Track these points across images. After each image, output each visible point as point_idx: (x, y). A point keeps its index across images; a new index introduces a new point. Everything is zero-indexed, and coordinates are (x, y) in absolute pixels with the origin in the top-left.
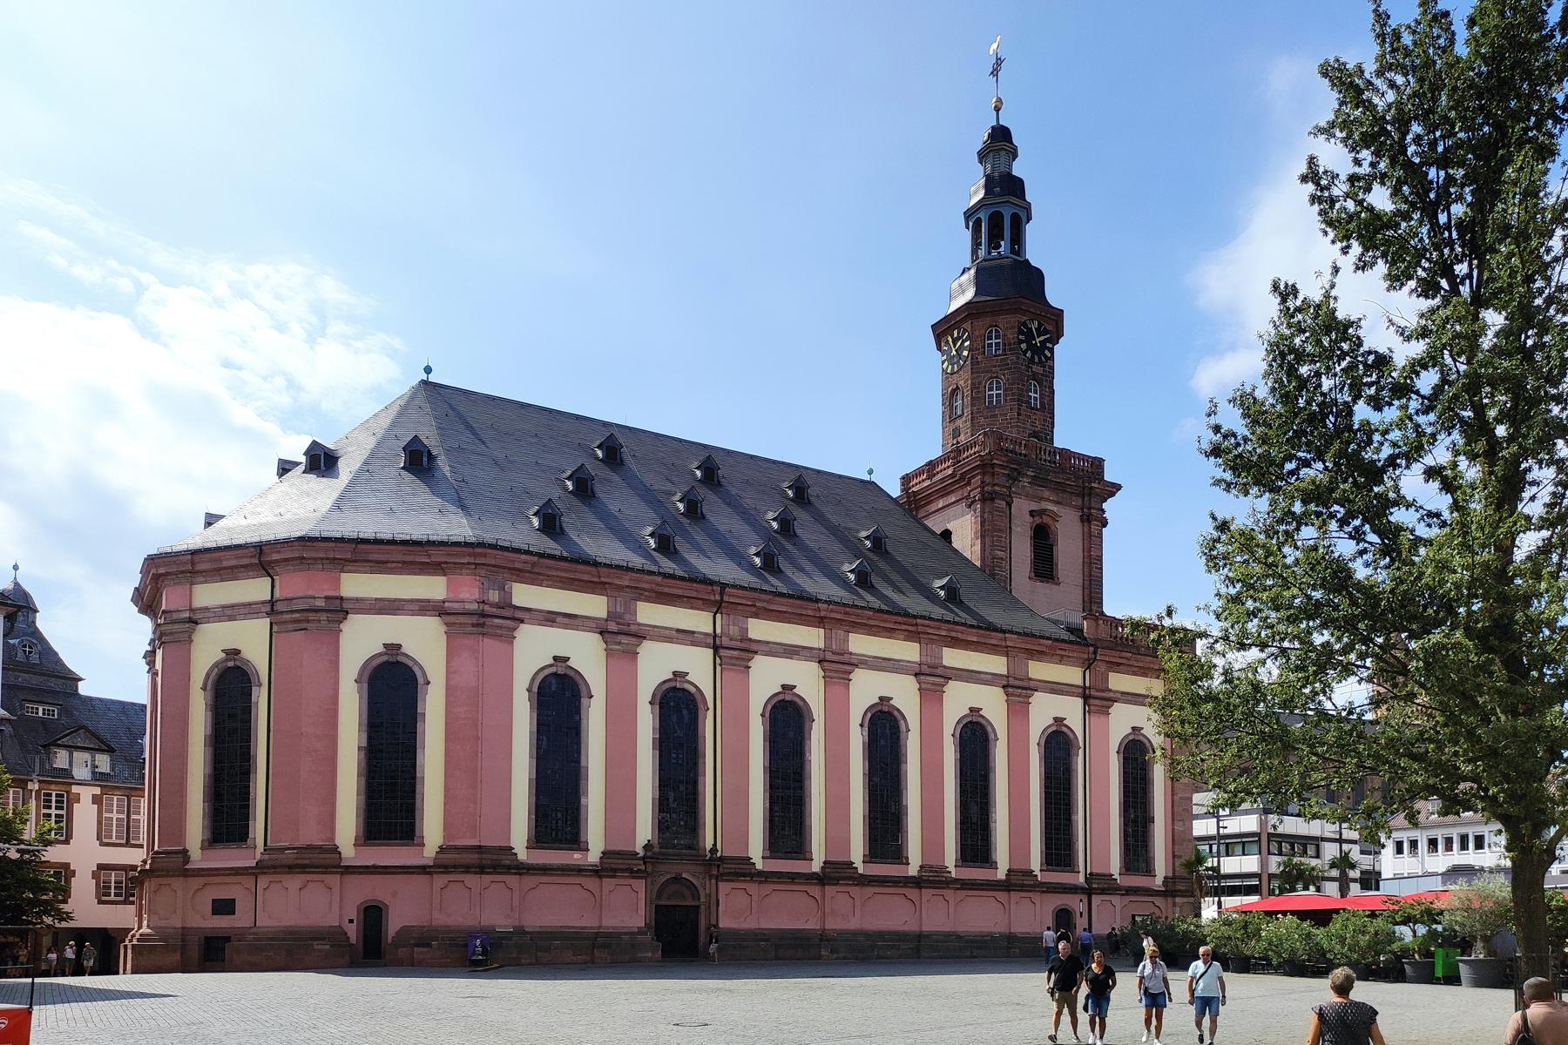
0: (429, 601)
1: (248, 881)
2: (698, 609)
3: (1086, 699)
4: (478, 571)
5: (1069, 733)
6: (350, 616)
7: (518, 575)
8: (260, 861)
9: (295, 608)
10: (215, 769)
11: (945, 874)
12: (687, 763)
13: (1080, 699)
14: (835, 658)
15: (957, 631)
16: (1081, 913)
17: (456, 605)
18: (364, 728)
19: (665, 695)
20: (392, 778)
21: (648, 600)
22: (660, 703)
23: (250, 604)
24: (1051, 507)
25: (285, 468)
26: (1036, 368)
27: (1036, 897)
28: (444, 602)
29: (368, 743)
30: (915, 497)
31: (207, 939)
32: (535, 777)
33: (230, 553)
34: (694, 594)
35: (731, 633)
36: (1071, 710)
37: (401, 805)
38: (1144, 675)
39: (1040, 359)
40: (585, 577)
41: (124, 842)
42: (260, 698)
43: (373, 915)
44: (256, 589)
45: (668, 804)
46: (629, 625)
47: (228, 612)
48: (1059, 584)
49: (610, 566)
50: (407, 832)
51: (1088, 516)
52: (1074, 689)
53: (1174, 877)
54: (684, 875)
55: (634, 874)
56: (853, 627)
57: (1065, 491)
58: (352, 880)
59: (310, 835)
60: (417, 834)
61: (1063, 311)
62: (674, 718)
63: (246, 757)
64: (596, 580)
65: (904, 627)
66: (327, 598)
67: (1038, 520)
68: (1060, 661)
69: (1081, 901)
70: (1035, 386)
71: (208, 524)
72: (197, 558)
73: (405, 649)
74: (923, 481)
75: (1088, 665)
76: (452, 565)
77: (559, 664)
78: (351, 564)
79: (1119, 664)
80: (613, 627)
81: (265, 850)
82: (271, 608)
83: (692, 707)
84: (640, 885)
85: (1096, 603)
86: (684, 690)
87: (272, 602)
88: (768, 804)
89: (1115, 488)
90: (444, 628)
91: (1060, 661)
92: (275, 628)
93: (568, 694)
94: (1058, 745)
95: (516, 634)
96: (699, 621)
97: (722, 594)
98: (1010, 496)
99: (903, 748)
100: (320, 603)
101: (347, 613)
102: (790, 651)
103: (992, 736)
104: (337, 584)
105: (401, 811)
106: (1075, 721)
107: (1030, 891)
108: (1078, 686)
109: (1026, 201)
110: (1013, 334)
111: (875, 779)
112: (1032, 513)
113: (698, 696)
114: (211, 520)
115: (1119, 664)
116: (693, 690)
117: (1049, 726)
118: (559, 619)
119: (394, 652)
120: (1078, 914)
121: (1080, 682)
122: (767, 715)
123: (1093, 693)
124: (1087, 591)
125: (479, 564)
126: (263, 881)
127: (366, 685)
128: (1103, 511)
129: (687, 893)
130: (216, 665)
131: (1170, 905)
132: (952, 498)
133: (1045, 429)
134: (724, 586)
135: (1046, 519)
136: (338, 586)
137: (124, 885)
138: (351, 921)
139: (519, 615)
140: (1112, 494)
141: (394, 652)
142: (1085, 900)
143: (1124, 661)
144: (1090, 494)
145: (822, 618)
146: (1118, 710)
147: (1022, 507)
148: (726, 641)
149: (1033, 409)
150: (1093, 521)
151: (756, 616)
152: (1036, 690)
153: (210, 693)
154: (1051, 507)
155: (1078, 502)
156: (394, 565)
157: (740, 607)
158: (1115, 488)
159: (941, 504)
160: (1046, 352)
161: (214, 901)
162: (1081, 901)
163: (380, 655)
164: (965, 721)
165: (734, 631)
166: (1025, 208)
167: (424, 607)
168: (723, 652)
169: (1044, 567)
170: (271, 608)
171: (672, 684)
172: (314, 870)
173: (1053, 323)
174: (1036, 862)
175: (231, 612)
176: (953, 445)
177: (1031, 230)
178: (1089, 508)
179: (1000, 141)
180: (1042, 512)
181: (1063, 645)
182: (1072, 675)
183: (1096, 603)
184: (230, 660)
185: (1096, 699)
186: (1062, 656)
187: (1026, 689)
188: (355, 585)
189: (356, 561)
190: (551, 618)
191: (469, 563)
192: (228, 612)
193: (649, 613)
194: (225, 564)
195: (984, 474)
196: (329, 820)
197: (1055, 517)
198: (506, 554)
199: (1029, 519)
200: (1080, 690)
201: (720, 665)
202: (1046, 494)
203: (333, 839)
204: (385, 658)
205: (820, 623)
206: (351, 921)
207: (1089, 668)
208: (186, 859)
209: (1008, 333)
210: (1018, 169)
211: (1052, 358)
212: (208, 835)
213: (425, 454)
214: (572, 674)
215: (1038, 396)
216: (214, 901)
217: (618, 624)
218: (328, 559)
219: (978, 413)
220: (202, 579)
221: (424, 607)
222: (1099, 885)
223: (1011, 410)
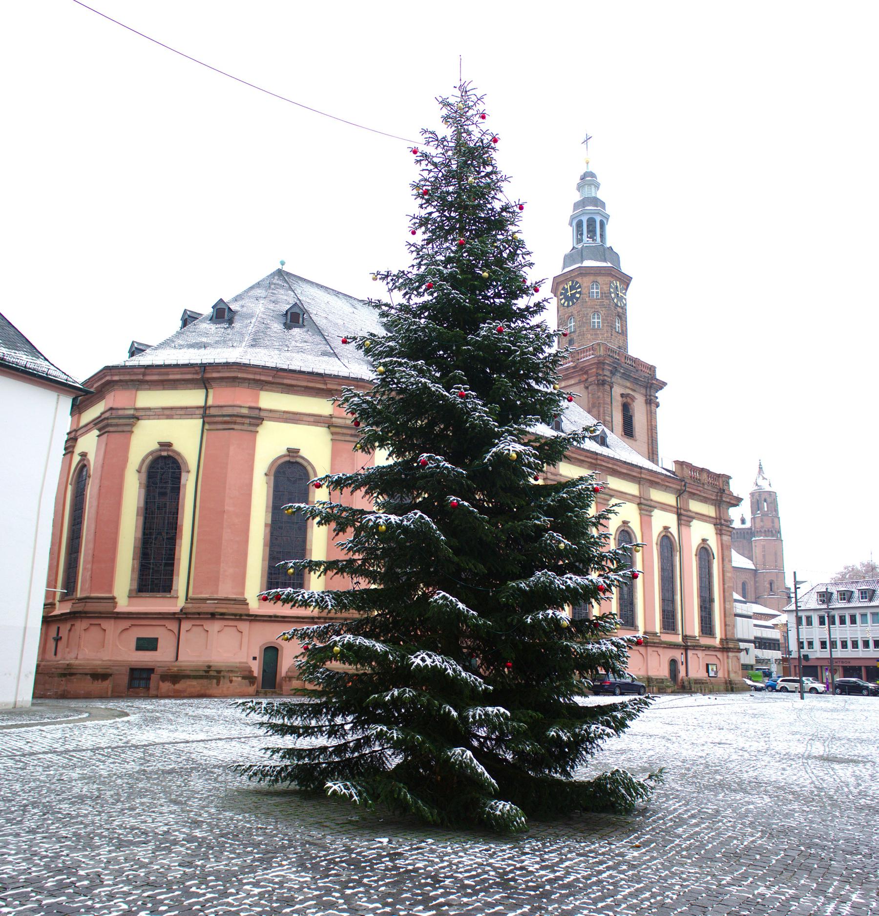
0: (321, 416)
1: (173, 625)
3: (679, 515)
5: (672, 537)
6: (265, 422)
9: (225, 413)
10: (144, 534)
15: (618, 466)
16: (682, 662)
17: (340, 421)
18: (270, 510)
23: (186, 408)
25: (189, 319)
27: (660, 651)
28: (332, 418)
29: (272, 521)
31: (133, 670)
33: (178, 370)
36: (670, 520)
44: (194, 398)
47: (167, 412)
48: (636, 440)
53: (726, 639)
58: (258, 627)
59: (226, 590)
60: (174, 588)
65: (590, 460)
66: (250, 408)
67: (625, 400)
69: (682, 654)
71: (132, 354)
72: (148, 371)
73: (302, 453)
75: (679, 494)
79: (694, 494)
82: (205, 413)
87: (205, 408)
89: (663, 384)
90: (329, 437)
92: (207, 427)
94: (668, 545)
100: (245, 411)
101: (263, 420)
104: (257, 399)
107: (657, 647)
112: (622, 395)
114: (135, 350)
119: (295, 455)
124: (650, 447)
126: (186, 625)
127: (272, 478)
130: (151, 453)
131: (725, 657)
132: (572, 382)
135: (629, 400)
136: (257, 400)
138: (255, 658)
140: (661, 388)
141: (295, 455)
143: (698, 492)
144: (651, 387)
146: (695, 523)
149: (618, 333)
150: (651, 402)
153: (144, 475)
155: (643, 391)
156: (299, 388)
158: (663, 384)
161: (138, 639)
163: (284, 456)
167: (316, 420)
170: (205, 413)
173: (107, 368)
174: (658, 628)
175: (168, 413)
177: (608, 228)
178: (650, 396)
179: (588, 179)
180: (628, 395)
184: (164, 450)
185: (684, 517)
186: (667, 486)
187: (651, 506)
188: (269, 400)
192: (167, 412)
194: (171, 377)
195: (597, 368)
196: (241, 579)
197: (633, 399)
199: (620, 399)
200: (675, 510)
203: (243, 594)
204: (287, 459)
206: (255, 658)
207: (679, 496)
210: (601, 195)
212: (135, 586)
216: (138, 639)
220: (147, 387)
221: (316, 420)
222: (688, 645)
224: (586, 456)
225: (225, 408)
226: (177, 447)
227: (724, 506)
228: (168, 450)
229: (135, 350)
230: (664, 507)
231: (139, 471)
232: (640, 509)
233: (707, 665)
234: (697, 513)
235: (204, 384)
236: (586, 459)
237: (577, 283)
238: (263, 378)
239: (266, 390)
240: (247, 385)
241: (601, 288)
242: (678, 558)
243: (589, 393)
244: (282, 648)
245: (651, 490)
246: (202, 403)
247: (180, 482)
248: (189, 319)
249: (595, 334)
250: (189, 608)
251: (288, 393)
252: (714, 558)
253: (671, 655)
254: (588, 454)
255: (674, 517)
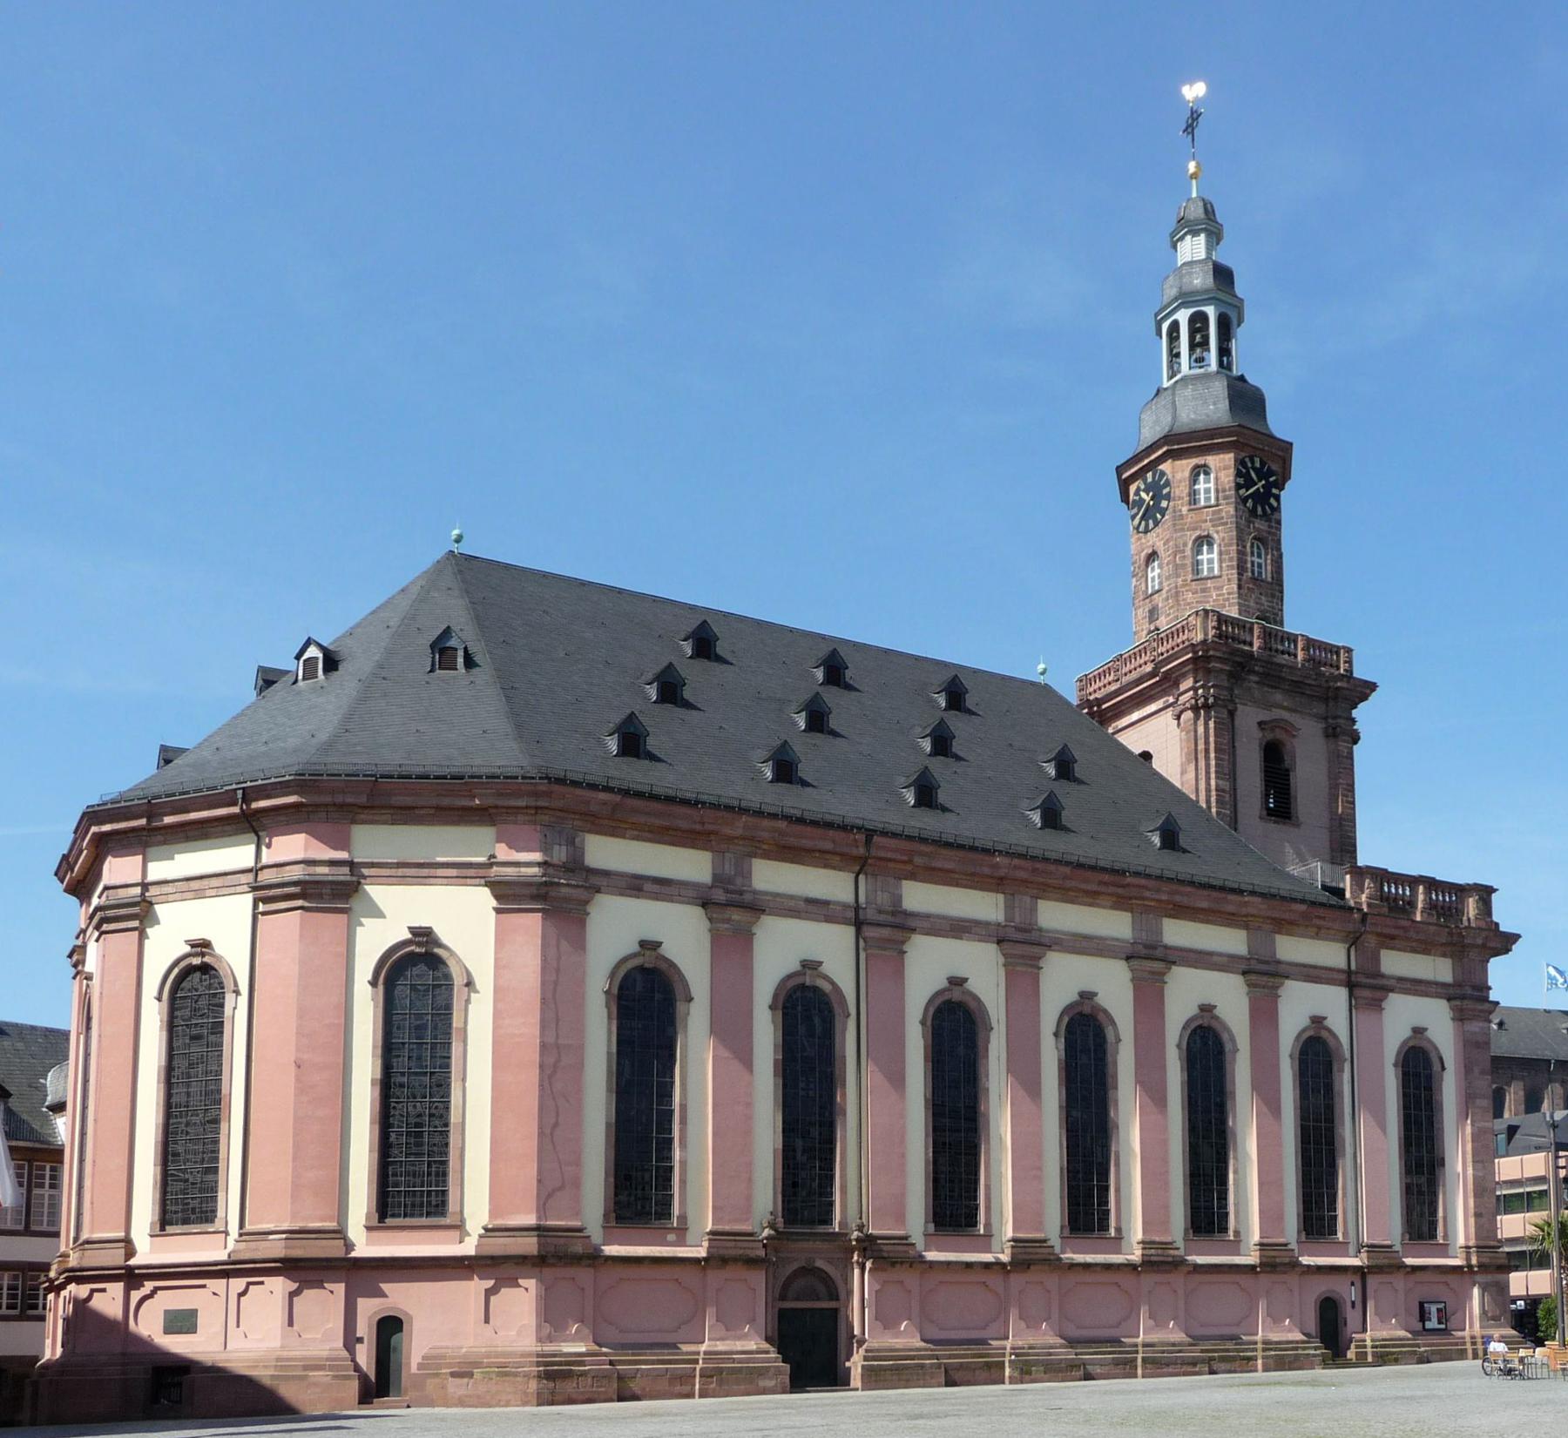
2: (834, 868)
4: (540, 817)
7: (593, 823)
8: (233, 1251)
11: (1171, 1252)
12: (821, 1097)
13: (1343, 989)
14: (1019, 936)
16: (1353, 1303)
19: (791, 996)
20: (417, 1125)
21: (767, 856)
22: (784, 1007)
24: (1285, 715)
25: (268, 679)
26: (1260, 525)
30: (1099, 706)
32: (614, 1121)
34: (828, 846)
35: (879, 902)
36: (1331, 1003)
37: (429, 1165)
38: (1426, 952)
39: (1264, 510)
40: (684, 824)
41: (21, 1227)
42: (236, 1011)
43: (360, 1340)
45: (795, 1158)
46: (741, 893)
48: (1297, 825)
49: (716, 806)
50: (437, 1206)
51: (1334, 729)
52: (1336, 976)
54: (819, 1264)
55: (751, 1262)
56: (1044, 891)
57: (1303, 693)
60: (452, 1206)
61: (1291, 444)
62: (802, 1029)
63: (214, 1098)
64: (698, 827)
65: (1111, 889)
67: (1270, 736)
68: (1317, 934)
70: (1258, 548)
74: (1110, 683)
75: (1354, 941)
76: (504, 810)
77: (648, 953)
78: (366, 812)
79: (1393, 938)
80: (719, 895)
81: (241, 1235)
83: (826, 1012)
84: (758, 1279)
85: (1349, 852)
86: (816, 989)
87: (256, 871)
88: (931, 1154)
89: (1365, 689)
91: (1317, 934)
93: (657, 996)
95: (590, 908)
96: (834, 885)
97: (868, 842)
98: (1232, 701)
99: (1110, 1066)
102: (958, 928)
103: (1228, 1047)
105: (429, 1174)
106: (1338, 1023)
108: (1339, 971)
109: (1236, 297)
110: (1228, 476)
111: (1074, 1113)
112: (1261, 725)
113: (834, 999)
115: (1393, 938)
116: (827, 987)
117: (1304, 1030)
118: (648, 887)
120: (1349, 1304)
121: (1342, 964)
122: (929, 1023)
123: (1362, 980)
125: (541, 808)
128: (1353, 721)
129: (821, 1288)
132: (1153, 707)
133: (1273, 608)
134: (870, 834)
137: (20, 1292)
139: (595, 880)
140: (1364, 698)
142: (1358, 1284)
144: (1336, 698)
145: (1001, 879)
147: (1249, 717)
148: (871, 914)
150: (1342, 735)
151: (912, 876)
152: (1287, 977)
154: (1285, 715)
155: (1319, 708)
157: (891, 865)
158: (1365, 689)
159: (1135, 716)
160: (1272, 501)
161: (167, 1312)
162: (1353, 1284)
164: (1193, 1026)
165: (883, 899)
166: (1236, 306)
167: (465, 873)
168: (869, 932)
169: (1280, 806)
171: (799, 980)
172: (258, 1265)
175: (196, 886)
176: (1150, 632)
181: (1321, 912)
182: (1331, 954)
183: (1349, 852)
186: (1319, 928)
189: (372, 807)
190: (636, 886)
191: (527, 807)
193: (770, 876)
198: (578, 792)
199: (1257, 734)
200: (1343, 977)
201: (865, 950)
202: (1278, 697)
205: (999, 884)
208: (130, 1252)
209: (1222, 474)
211: (1277, 510)
213: (461, 653)
214: (664, 966)
215: (1262, 561)
216: (167, 1312)
217: (727, 891)
218: (335, 805)
219: (1183, 586)
220: (160, 838)
223: (1229, 580)
224: (1101, 883)
225: (288, 868)
226: (219, 948)
227: (1473, 954)
228: (203, 955)
229: (168, 756)
230: (1314, 974)
231: (159, 999)
232: (1250, 985)
233: (1421, 1305)
234: (1401, 979)
235: (249, 822)
236: (1102, 889)
237: (1163, 474)
238: (350, 800)
239: (364, 822)
240: (323, 815)
241: (1217, 479)
242: (1346, 1076)
243: (1182, 731)
244: (411, 1318)
245: (1278, 937)
246: (250, 863)
247: (223, 1012)
248: (268, 679)
249: (1204, 590)
250: (240, 1251)
251: (433, 825)
252: (1443, 1068)
253: (1324, 1289)
254: (1106, 877)
255: (1341, 993)
